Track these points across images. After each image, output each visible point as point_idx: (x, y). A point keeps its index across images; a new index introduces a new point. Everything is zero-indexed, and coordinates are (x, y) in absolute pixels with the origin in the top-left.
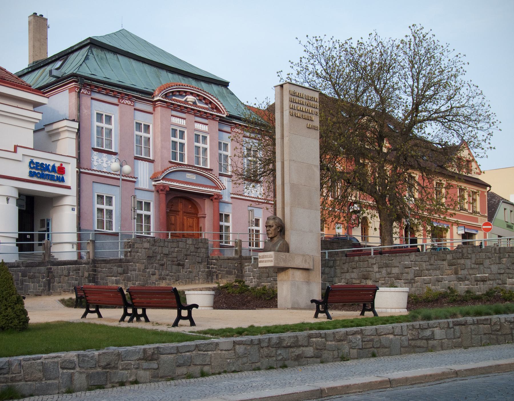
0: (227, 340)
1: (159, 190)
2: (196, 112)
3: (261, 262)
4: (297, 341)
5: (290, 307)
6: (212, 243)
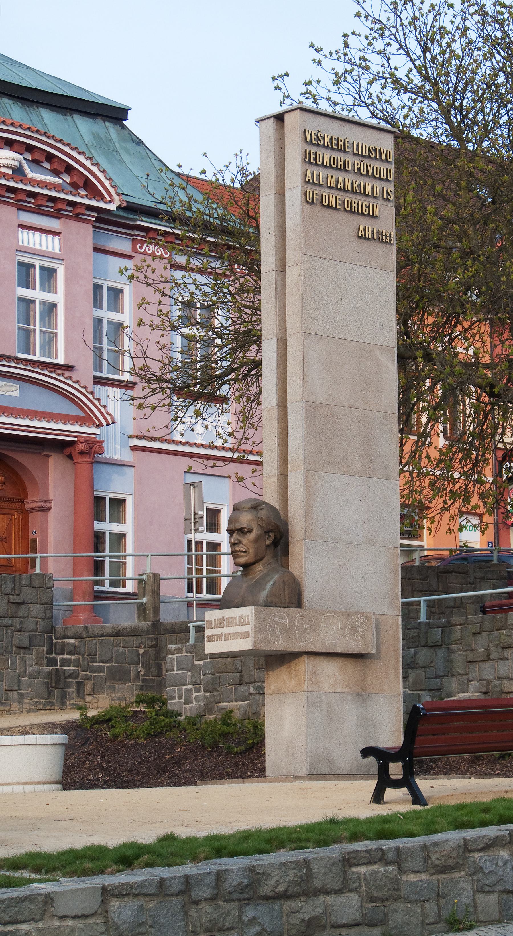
0: (83, 885)
2: (23, 197)
3: (212, 638)
4: (309, 876)
5: (304, 771)
6: (70, 586)
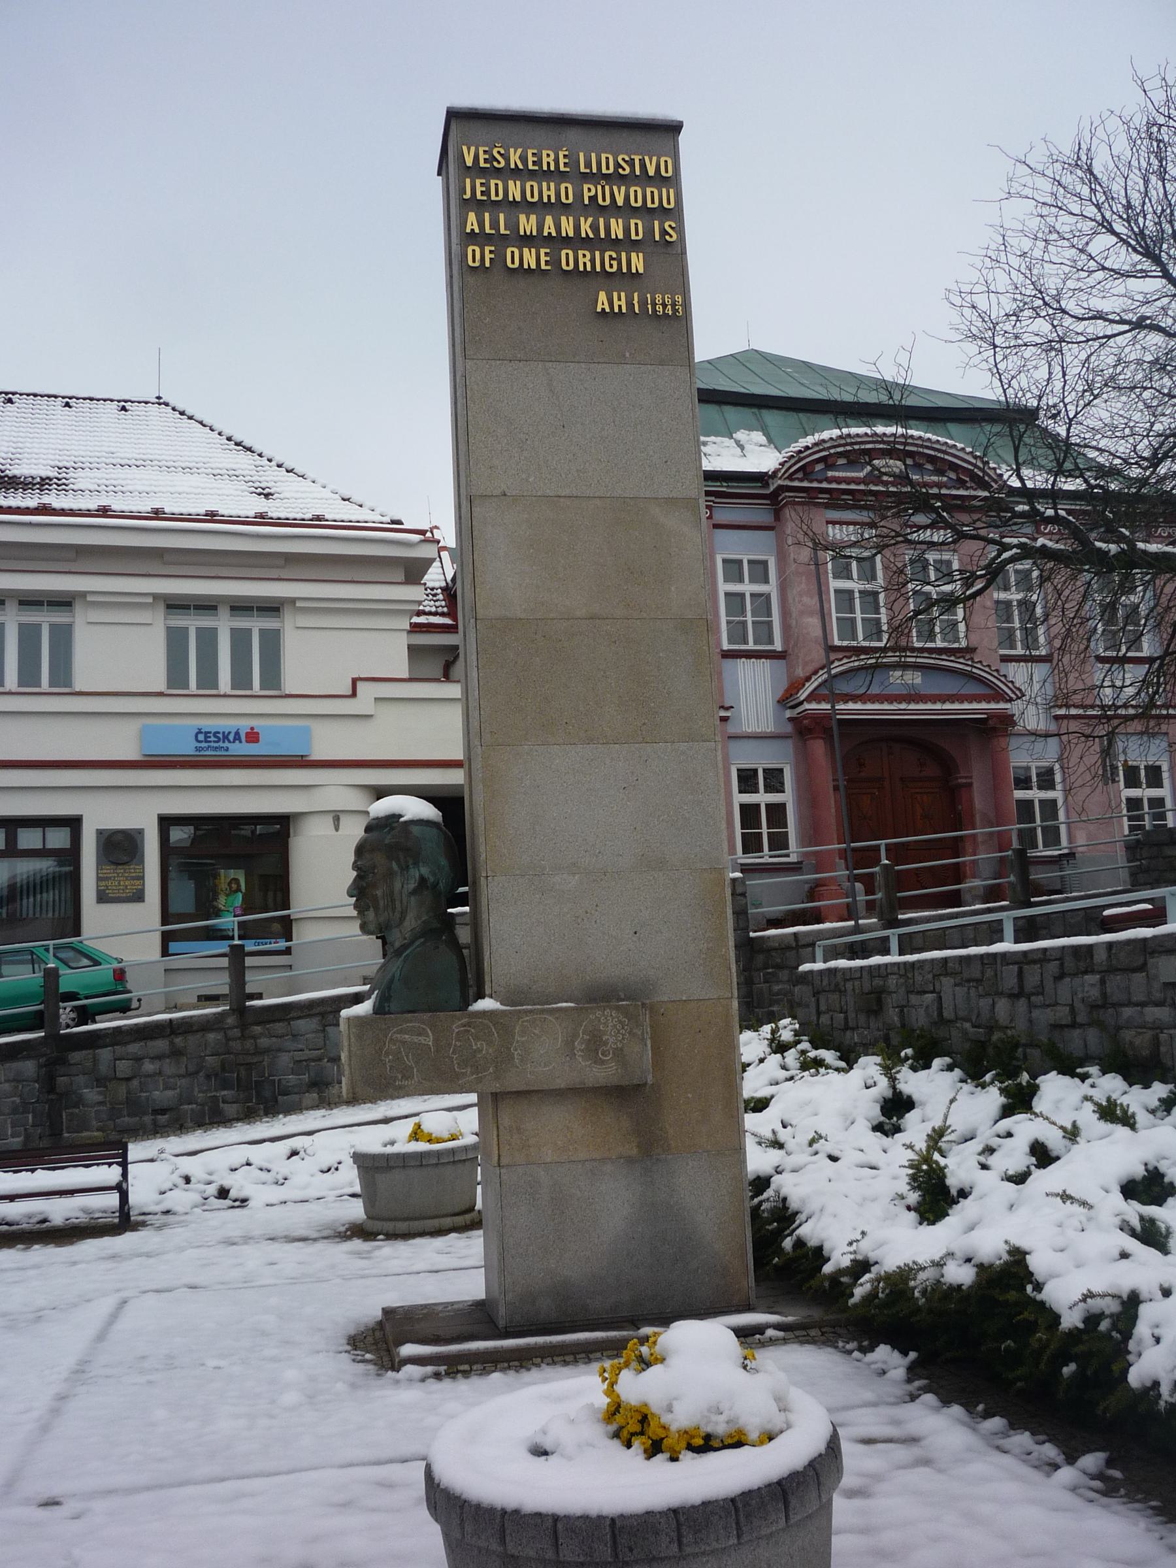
1: (805, 729)
2: (858, 496)
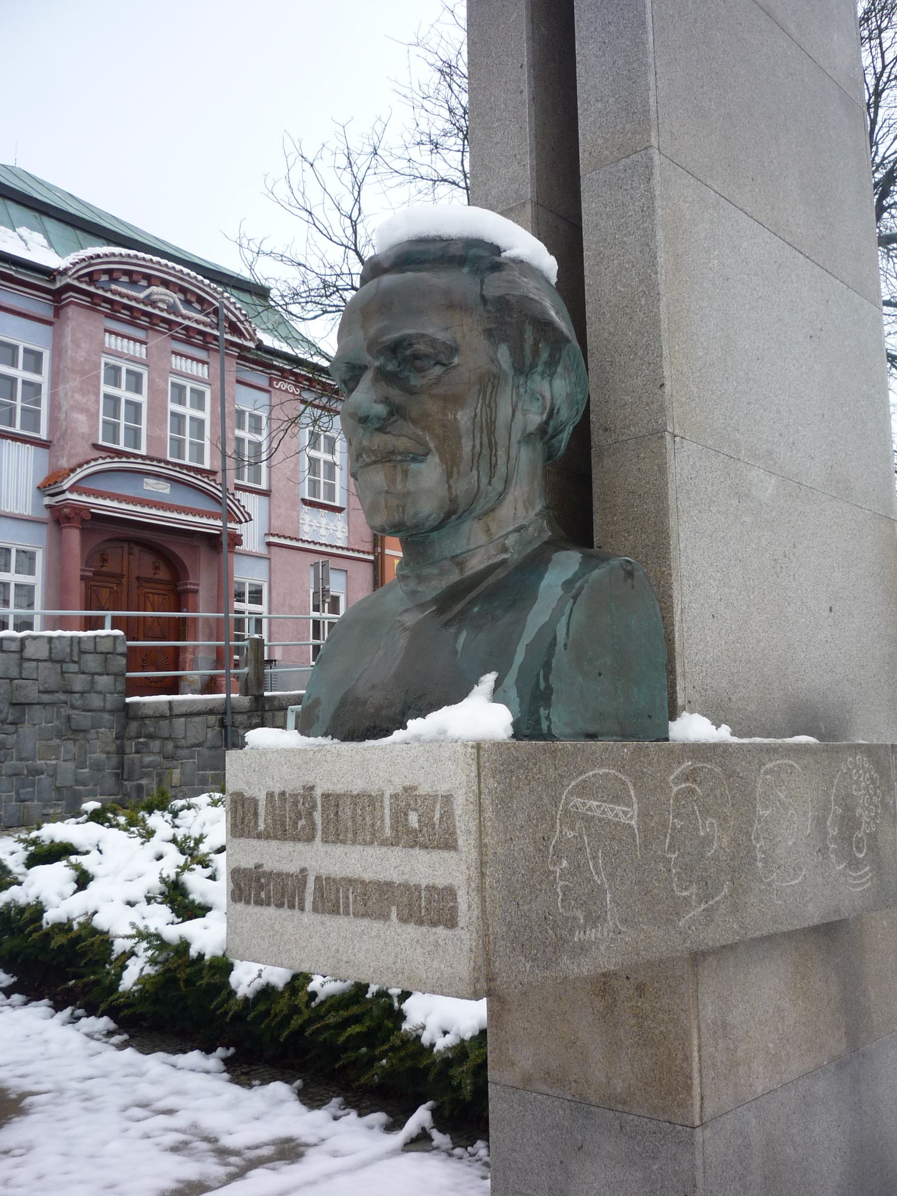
1: (61, 517)
